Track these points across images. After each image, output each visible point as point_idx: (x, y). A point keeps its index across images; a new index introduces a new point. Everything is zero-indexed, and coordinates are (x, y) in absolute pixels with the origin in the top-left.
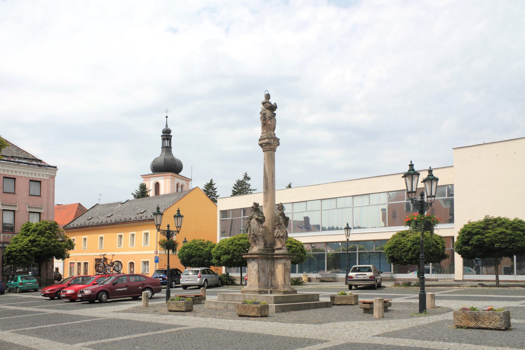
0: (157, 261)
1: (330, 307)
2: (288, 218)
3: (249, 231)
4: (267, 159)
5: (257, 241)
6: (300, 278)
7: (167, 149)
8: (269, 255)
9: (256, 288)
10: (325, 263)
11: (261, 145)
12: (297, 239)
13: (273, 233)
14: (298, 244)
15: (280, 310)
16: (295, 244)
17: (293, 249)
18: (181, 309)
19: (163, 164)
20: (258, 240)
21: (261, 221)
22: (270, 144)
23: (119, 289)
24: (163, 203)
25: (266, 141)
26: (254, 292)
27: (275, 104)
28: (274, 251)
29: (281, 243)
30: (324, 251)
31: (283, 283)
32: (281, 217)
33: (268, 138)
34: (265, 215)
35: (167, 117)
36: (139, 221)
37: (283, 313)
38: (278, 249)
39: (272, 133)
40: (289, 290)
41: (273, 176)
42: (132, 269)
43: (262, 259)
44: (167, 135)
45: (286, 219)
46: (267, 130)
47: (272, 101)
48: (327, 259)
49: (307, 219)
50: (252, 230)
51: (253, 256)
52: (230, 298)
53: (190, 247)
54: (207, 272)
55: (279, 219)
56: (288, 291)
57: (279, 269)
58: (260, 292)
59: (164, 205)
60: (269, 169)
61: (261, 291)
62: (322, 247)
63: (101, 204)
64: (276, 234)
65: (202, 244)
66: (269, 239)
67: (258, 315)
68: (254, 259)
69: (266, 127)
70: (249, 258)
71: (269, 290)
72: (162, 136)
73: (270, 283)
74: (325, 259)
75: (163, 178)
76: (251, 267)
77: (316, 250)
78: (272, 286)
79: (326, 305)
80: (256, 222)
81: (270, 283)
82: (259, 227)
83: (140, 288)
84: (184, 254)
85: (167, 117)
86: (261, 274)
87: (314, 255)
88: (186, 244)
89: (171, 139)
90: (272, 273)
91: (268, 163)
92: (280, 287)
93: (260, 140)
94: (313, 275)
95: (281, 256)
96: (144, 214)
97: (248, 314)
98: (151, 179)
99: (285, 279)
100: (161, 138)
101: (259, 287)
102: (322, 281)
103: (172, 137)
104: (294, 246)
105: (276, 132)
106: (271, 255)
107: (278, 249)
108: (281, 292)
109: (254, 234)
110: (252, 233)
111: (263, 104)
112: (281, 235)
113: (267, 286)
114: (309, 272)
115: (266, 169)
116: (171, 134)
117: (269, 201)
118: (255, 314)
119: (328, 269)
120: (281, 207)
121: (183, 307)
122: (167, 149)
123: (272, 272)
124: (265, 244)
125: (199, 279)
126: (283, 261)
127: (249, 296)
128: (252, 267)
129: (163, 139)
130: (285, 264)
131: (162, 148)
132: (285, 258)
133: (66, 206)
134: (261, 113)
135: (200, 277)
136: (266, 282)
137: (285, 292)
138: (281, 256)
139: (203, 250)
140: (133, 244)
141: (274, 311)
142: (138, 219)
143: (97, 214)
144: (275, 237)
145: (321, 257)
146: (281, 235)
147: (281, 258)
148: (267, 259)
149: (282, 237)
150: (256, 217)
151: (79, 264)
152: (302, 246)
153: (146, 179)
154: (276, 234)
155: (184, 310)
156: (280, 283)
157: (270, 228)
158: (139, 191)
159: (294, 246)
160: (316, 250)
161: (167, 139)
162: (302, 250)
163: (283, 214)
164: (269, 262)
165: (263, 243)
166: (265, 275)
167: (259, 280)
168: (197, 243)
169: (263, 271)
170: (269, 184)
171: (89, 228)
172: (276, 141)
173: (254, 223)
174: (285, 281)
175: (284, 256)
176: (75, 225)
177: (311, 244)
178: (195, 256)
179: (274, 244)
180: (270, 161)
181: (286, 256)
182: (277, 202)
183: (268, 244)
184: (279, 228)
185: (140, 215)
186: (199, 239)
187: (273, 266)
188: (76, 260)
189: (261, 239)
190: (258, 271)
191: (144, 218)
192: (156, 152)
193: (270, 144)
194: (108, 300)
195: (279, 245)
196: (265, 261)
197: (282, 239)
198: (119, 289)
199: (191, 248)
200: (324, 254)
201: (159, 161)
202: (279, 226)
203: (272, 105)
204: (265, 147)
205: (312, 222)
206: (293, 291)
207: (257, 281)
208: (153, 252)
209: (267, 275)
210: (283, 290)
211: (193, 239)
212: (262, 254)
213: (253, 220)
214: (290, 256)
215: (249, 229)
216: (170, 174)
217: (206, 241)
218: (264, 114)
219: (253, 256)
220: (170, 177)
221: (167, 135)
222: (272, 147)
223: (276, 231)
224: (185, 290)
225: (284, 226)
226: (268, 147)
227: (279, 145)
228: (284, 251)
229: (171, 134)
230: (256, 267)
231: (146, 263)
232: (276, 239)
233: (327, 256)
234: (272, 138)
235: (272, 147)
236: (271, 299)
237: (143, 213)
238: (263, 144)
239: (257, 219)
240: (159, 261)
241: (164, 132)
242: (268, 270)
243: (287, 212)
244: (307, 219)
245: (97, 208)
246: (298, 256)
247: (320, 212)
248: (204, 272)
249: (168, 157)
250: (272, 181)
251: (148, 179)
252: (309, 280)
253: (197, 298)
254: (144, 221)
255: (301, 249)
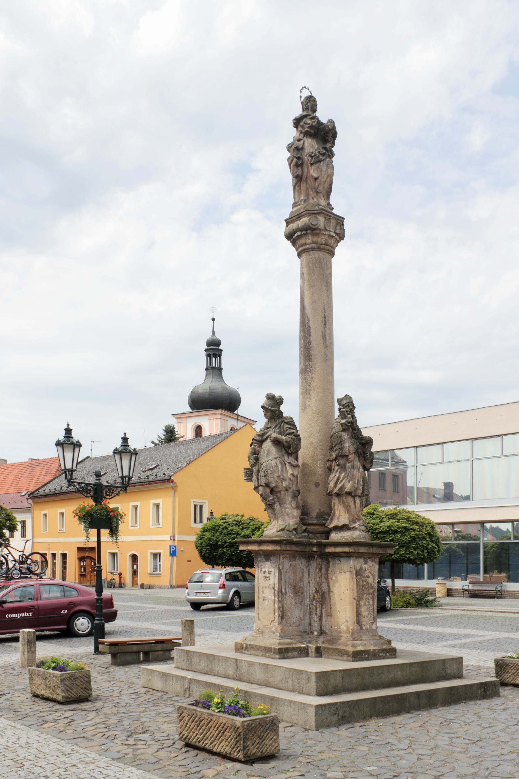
0: (173, 553)
1: (496, 694)
2: (369, 442)
3: (254, 478)
4: (309, 274)
5: (277, 506)
6: (427, 592)
7: (215, 371)
8: (313, 545)
9: (273, 641)
10: (479, 560)
11: (290, 236)
12: (422, 515)
13: (327, 483)
14: (421, 523)
15: (334, 719)
16: (417, 523)
17: (413, 533)
18: (55, 696)
19: (207, 394)
20: (281, 503)
21: (289, 447)
22: (315, 233)
23: (14, 615)
24: (189, 452)
25: (305, 220)
26: (267, 651)
27: (332, 122)
28: (327, 533)
29: (348, 511)
30: (478, 539)
31: (353, 626)
32: (345, 436)
33: (308, 213)
34: (301, 433)
35: (213, 320)
36: (145, 483)
37: (343, 728)
38: (337, 528)
39: (323, 202)
40: (371, 648)
41: (327, 322)
42: (135, 567)
43: (293, 556)
44: (214, 349)
45: (364, 444)
46: (308, 195)
47: (323, 115)
48: (485, 553)
49: (448, 486)
50: (262, 473)
51: (265, 548)
52: (203, 665)
53: (214, 529)
54: (240, 578)
55: (341, 443)
56: (366, 652)
57: (343, 584)
58: (284, 653)
59: (190, 456)
60: (313, 303)
61: (287, 650)
62: (472, 530)
63: (92, 457)
64: (332, 485)
65: (238, 523)
66: (315, 501)
67: (235, 755)
68: (268, 556)
69: (304, 186)
70: (257, 552)
71: (312, 647)
72: (206, 350)
73: (316, 626)
74: (479, 553)
75: (207, 418)
76: (261, 580)
77: (463, 538)
78: (322, 632)
79: (485, 691)
80: (274, 450)
81: (316, 626)
82: (284, 464)
83: (64, 612)
84: (205, 541)
85: (213, 320)
86: (290, 600)
87: (458, 545)
88: (213, 522)
89: (220, 356)
90: (323, 597)
91: (311, 286)
92: (345, 637)
93: (288, 222)
94: (457, 584)
95: (346, 549)
96: (154, 471)
97: (207, 744)
98: (188, 420)
99: (358, 614)
100: (204, 353)
101: (282, 637)
102: (474, 595)
103: (223, 353)
104: (415, 527)
105: (333, 200)
106: (320, 545)
107: (337, 528)
108: (346, 653)
109: (267, 485)
110: (263, 481)
111: (297, 122)
112: (347, 490)
113: (306, 633)
114: (448, 577)
115: (307, 303)
116: (221, 347)
117: (313, 394)
118: (228, 749)
119: (485, 572)
120: (348, 407)
121: (59, 691)
122: (215, 371)
123: (323, 595)
124: (304, 513)
125: (221, 591)
126: (353, 563)
127: (251, 664)
128: (265, 578)
129: (209, 356)
130: (359, 573)
131: (207, 369)
132: (359, 555)
133: (42, 461)
134: (289, 148)
135: (224, 586)
136: (307, 622)
137: (358, 656)
138: (346, 549)
139: (238, 534)
140: (136, 523)
141: (313, 724)
142: (142, 480)
143: (84, 473)
144: (329, 494)
145: (472, 550)
146: (348, 487)
147: (348, 555)
148: (309, 557)
149: (349, 494)
150: (274, 435)
151: (54, 555)
152: (433, 528)
153: (180, 420)
154: (332, 485)
155: (60, 698)
156: (343, 627)
157: (319, 469)
158: (163, 437)
159: (415, 527)
160: (463, 538)
161: (215, 356)
162: (432, 536)
163: (351, 427)
164: (314, 564)
165: (296, 513)
166: (302, 603)
167: (282, 617)
168: (230, 521)
169: (297, 591)
170: (313, 344)
171: (62, 497)
172: (333, 222)
173: (268, 454)
174: (358, 622)
175: (354, 550)
176: (47, 491)
177: (453, 524)
178: (222, 546)
179: (328, 513)
180: (318, 281)
181: (362, 550)
182: (339, 393)
183: (314, 514)
184: (343, 468)
185: (147, 473)
186: (235, 513)
187: (327, 578)
188: (49, 549)
189: (288, 498)
190: (280, 591)
191: (152, 478)
192: (195, 377)
193: (315, 233)
194: (22, 576)
195: (341, 517)
196: (301, 563)
197: (350, 500)
198: (10, 616)
199: (217, 530)
200: (479, 545)
201: (200, 391)
202: (341, 461)
203: (320, 123)
204: (302, 241)
205: (457, 490)
206: (384, 651)
207: (277, 620)
208: (168, 537)
209: (307, 601)
210: (351, 649)
211: (224, 513)
212: (290, 542)
213: (268, 445)
214: (375, 550)
215: (255, 469)
216: (219, 411)
217: (246, 517)
218: (298, 149)
219: (265, 548)
220: (219, 416)
221: (214, 349)
222: (322, 239)
223: (333, 477)
224: (197, 613)
225: (358, 464)
226: (309, 239)
227: (341, 237)
228: (357, 534)
229: (221, 347)
230: (274, 579)
231: (156, 556)
232: (335, 501)
233: (485, 547)
234: (321, 212)
235: (322, 239)
236: (309, 680)
237: (152, 469)
238: (295, 232)
239: (277, 442)
240: (178, 552)
241: (209, 344)
242: (310, 588)
243: (364, 420)
244: (448, 486)
245: (87, 463)
246: (423, 548)
247: (469, 463)
248: (232, 577)
249: (217, 386)
250: (324, 337)
251: (184, 420)
252: (450, 593)
253: (159, 647)
254: (153, 482)
255: (429, 534)
